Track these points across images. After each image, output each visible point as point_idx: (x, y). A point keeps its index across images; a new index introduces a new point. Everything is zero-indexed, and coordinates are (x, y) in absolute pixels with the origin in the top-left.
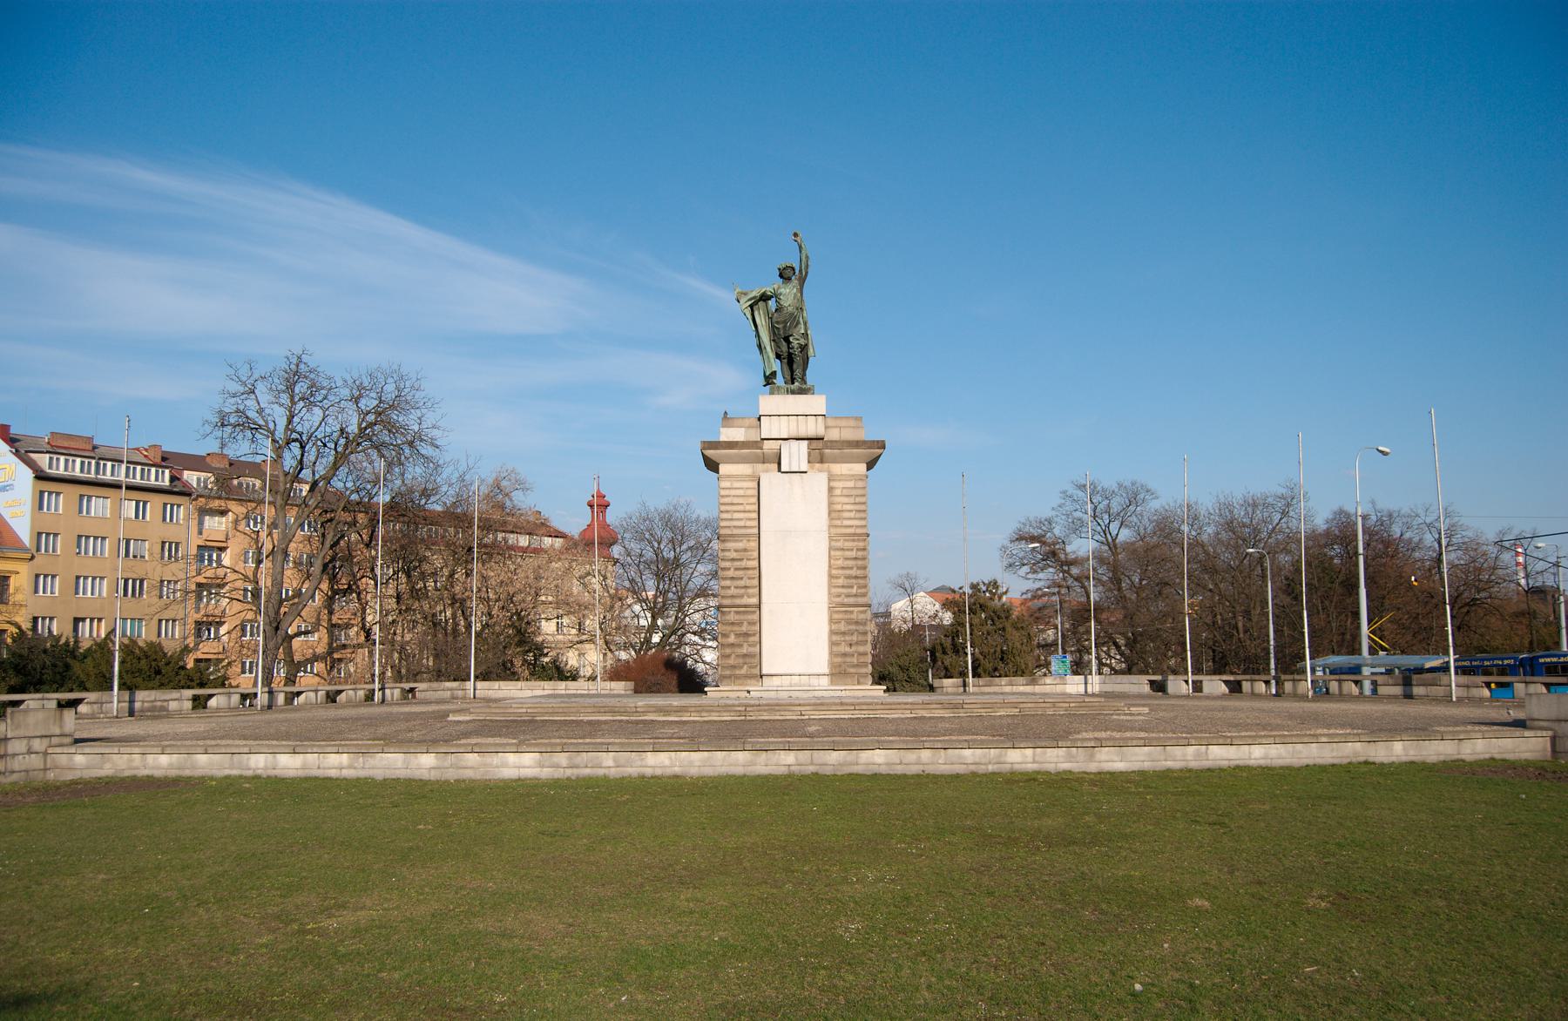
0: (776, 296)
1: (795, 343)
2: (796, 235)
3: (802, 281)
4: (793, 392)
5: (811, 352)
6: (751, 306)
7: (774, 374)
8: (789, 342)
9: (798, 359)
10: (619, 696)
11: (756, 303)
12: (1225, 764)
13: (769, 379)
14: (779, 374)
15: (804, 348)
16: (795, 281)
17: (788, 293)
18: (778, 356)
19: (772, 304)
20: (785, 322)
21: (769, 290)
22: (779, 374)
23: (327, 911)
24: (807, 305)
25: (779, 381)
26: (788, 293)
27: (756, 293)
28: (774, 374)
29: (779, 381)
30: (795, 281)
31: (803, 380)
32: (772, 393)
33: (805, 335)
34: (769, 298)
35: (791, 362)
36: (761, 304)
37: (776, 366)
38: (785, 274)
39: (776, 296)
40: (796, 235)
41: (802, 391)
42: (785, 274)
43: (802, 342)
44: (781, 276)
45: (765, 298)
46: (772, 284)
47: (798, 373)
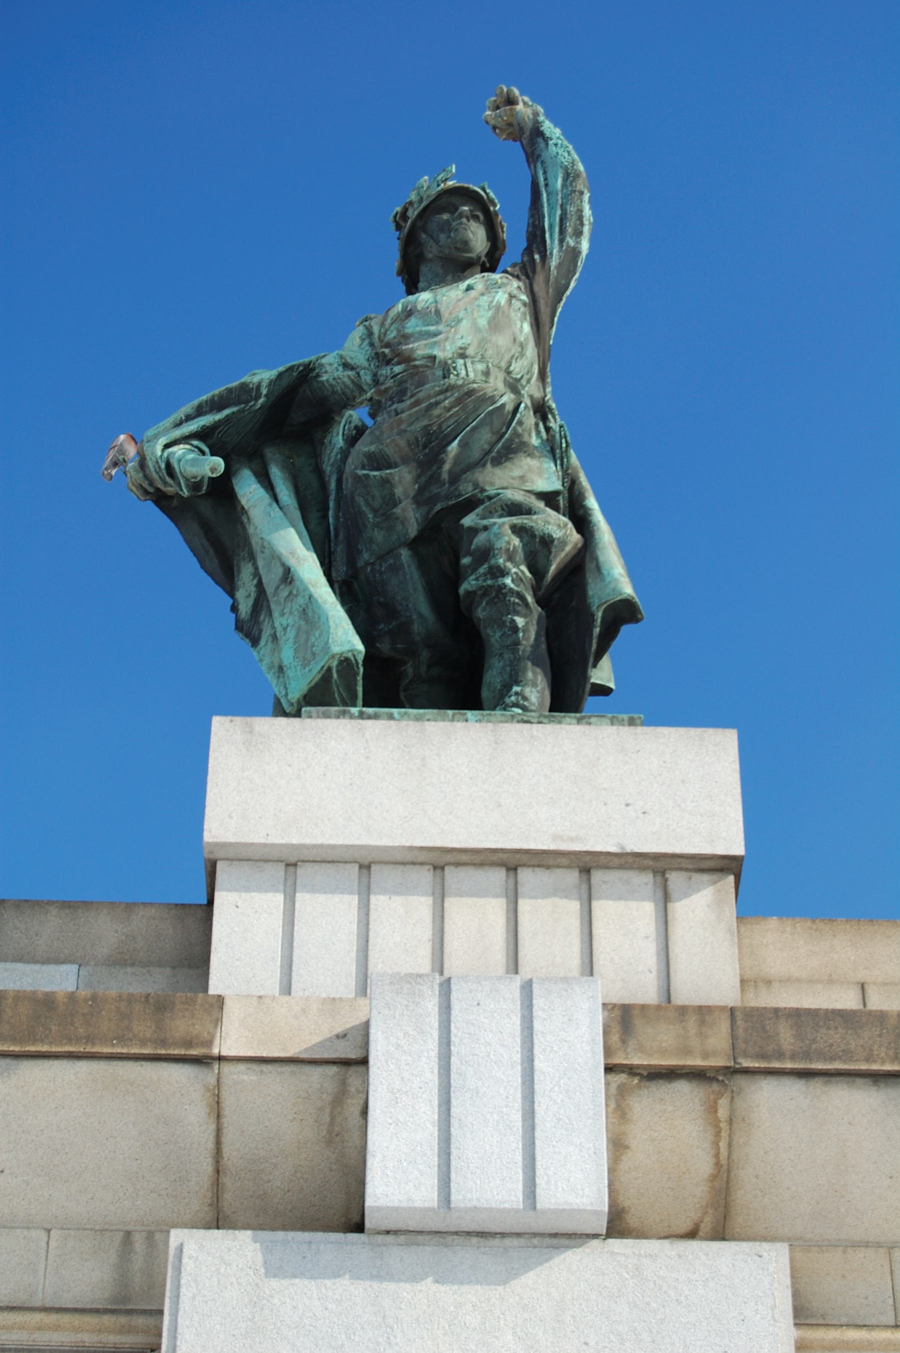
23: (518, 604)
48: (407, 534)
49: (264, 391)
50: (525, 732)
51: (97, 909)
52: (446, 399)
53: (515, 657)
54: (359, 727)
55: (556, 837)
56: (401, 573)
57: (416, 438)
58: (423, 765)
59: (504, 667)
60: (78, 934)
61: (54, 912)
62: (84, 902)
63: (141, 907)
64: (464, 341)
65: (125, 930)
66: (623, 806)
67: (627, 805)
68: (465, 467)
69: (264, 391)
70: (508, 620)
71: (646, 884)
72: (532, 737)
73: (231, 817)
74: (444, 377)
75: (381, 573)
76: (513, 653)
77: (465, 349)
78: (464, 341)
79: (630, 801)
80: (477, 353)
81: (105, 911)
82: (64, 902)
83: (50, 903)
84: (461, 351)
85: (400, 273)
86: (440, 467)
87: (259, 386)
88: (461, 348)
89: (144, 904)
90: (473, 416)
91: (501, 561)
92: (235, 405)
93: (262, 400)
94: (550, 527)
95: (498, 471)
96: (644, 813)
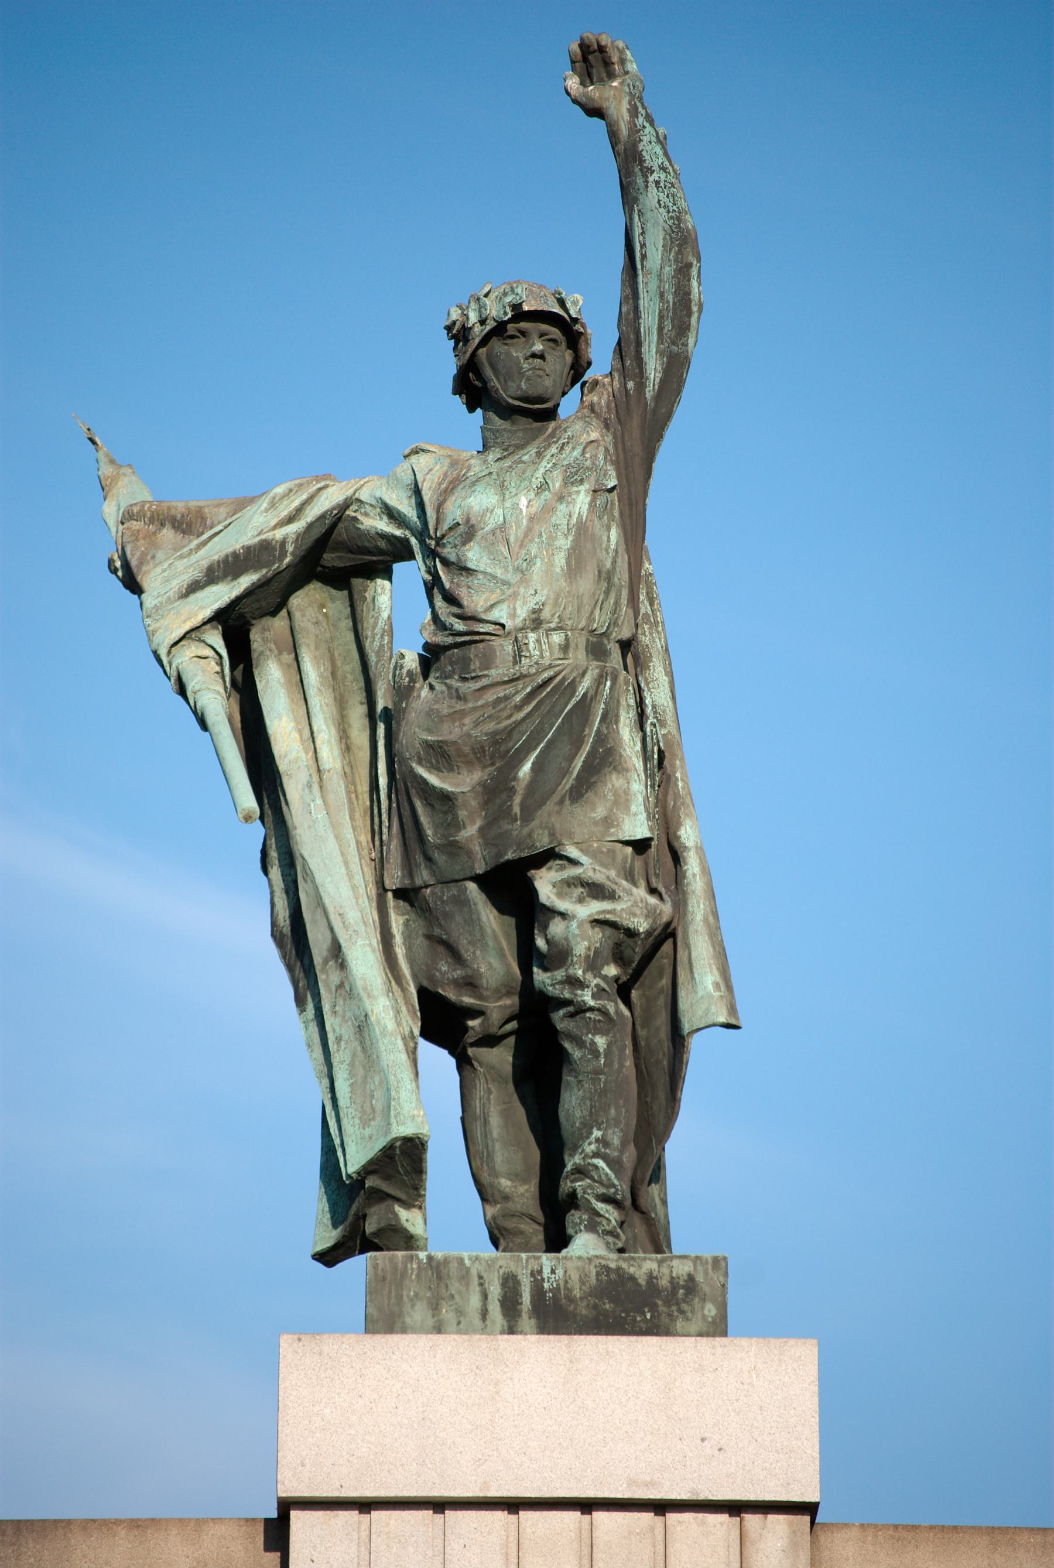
0: (427, 542)
1: (575, 922)
2: (593, 60)
3: (640, 427)
4: (555, 1315)
5: (701, 993)
6: (235, 626)
7: (403, 1163)
8: (523, 909)
9: (598, 1050)
10: (646, 864)
11: (272, 597)
12: (520, 1113)
13: (366, 1203)
14: (447, 1169)
15: (647, 958)
16: (581, 431)
17: (526, 528)
18: (442, 1021)
19: (398, 603)
20: (498, 753)
21: (376, 495)
22: (447, 1169)
23: (599, 1021)
24: (685, 620)
25: (449, 1216)
26: (526, 528)
27: (269, 520)
28: (404, 1161)
29: (449, 1216)
30: (581, 431)
31: (640, 1212)
32: (384, 1320)
33: (659, 856)
34: (378, 559)
35: (536, 1055)
36: (312, 605)
37: (425, 1094)
38: (505, 375)
39: (427, 542)
40: (593, 60)
41: (628, 1309)
42: (505, 375)
43: (636, 908)
44: (472, 387)
45: (339, 557)
46: (395, 445)
47: (597, 1153)
48: (473, 868)
49: (290, 548)
50: (600, 1346)
51: (166, 1530)
52: (517, 693)
53: (596, 1090)
54: (431, 1343)
55: (632, 1483)
56: (466, 909)
57: (483, 747)
58: (497, 1393)
59: (583, 1099)
60: (148, 1561)
61: (122, 1533)
62: (153, 1520)
63: (211, 1524)
64: (538, 598)
65: (196, 1554)
66: (699, 1441)
67: (703, 1440)
68: (537, 796)
69: (290, 548)
70: (588, 1041)
71: (722, 1524)
72: (607, 1353)
73: (303, 1465)
74: (515, 663)
75: (443, 902)
76: (593, 1084)
77: (540, 610)
78: (538, 598)
79: (706, 1435)
80: (552, 616)
81: (174, 1531)
82: (132, 1520)
83: (117, 1522)
84: (534, 616)
85: (457, 391)
86: (510, 798)
87: (283, 543)
88: (534, 611)
89: (213, 1519)
90: (545, 708)
91: (580, 972)
92: (256, 568)
93: (287, 560)
94: (636, 920)
95: (578, 810)
96: (720, 1450)
